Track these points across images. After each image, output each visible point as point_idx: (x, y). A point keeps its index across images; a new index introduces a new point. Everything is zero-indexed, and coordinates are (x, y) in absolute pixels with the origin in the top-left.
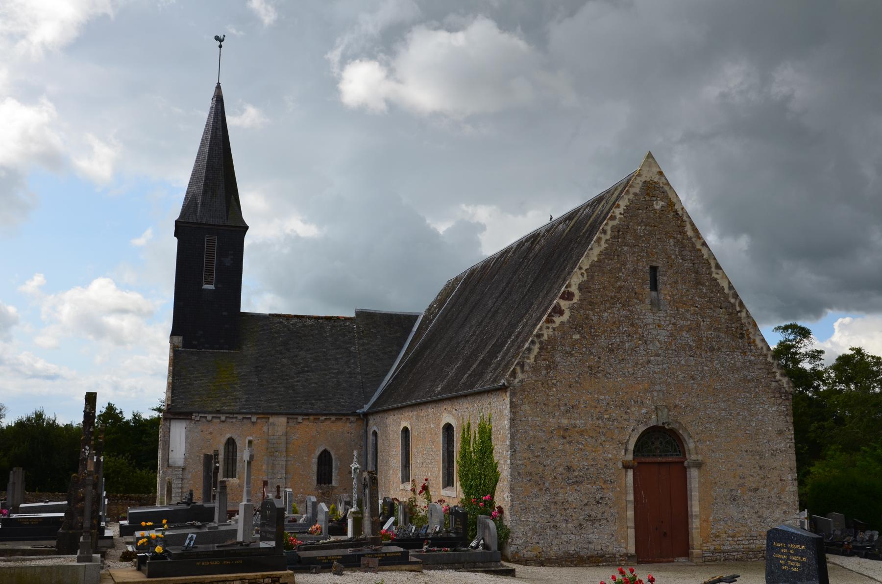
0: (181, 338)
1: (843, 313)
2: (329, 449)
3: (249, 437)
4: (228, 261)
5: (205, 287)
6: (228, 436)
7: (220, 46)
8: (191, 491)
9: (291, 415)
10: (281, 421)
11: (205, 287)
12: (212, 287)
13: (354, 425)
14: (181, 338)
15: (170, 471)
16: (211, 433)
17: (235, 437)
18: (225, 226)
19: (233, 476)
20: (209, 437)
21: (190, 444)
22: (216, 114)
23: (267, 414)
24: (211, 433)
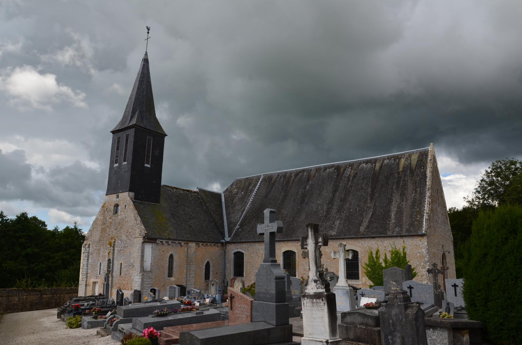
0: (133, 194)
1: (457, 159)
2: (210, 261)
3: (179, 252)
4: (157, 153)
5: (146, 165)
6: (171, 253)
7: (148, 33)
8: (208, 263)
9: (197, 242)
10: (193, 245)
11: (146, 165)
12: (149, 166)
13: (219, 248)
14: (133, 194)
15: (145, 274)
16: (163, 251)
17: (174, 254)
18: (157, 133)
19: (171, 277)
20: (162, 253)
21: (154, 257)
22: (143, 68)
23: (187, 241)
24: (163, 251)
